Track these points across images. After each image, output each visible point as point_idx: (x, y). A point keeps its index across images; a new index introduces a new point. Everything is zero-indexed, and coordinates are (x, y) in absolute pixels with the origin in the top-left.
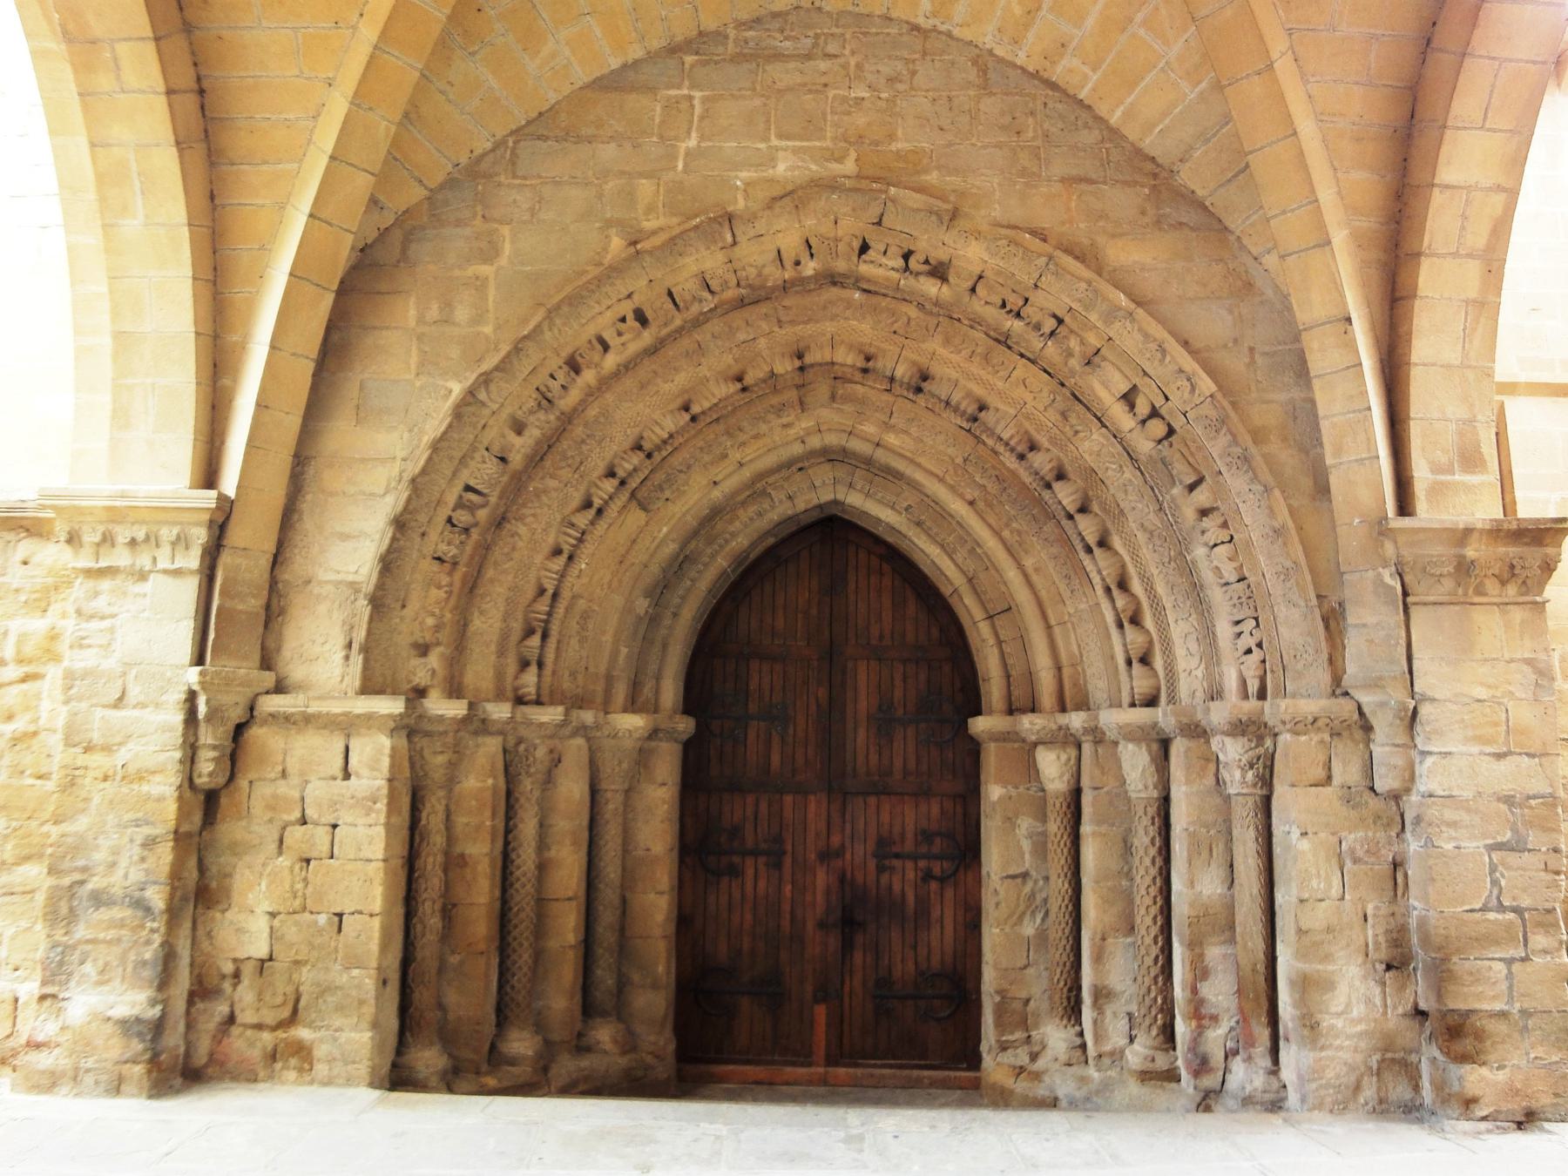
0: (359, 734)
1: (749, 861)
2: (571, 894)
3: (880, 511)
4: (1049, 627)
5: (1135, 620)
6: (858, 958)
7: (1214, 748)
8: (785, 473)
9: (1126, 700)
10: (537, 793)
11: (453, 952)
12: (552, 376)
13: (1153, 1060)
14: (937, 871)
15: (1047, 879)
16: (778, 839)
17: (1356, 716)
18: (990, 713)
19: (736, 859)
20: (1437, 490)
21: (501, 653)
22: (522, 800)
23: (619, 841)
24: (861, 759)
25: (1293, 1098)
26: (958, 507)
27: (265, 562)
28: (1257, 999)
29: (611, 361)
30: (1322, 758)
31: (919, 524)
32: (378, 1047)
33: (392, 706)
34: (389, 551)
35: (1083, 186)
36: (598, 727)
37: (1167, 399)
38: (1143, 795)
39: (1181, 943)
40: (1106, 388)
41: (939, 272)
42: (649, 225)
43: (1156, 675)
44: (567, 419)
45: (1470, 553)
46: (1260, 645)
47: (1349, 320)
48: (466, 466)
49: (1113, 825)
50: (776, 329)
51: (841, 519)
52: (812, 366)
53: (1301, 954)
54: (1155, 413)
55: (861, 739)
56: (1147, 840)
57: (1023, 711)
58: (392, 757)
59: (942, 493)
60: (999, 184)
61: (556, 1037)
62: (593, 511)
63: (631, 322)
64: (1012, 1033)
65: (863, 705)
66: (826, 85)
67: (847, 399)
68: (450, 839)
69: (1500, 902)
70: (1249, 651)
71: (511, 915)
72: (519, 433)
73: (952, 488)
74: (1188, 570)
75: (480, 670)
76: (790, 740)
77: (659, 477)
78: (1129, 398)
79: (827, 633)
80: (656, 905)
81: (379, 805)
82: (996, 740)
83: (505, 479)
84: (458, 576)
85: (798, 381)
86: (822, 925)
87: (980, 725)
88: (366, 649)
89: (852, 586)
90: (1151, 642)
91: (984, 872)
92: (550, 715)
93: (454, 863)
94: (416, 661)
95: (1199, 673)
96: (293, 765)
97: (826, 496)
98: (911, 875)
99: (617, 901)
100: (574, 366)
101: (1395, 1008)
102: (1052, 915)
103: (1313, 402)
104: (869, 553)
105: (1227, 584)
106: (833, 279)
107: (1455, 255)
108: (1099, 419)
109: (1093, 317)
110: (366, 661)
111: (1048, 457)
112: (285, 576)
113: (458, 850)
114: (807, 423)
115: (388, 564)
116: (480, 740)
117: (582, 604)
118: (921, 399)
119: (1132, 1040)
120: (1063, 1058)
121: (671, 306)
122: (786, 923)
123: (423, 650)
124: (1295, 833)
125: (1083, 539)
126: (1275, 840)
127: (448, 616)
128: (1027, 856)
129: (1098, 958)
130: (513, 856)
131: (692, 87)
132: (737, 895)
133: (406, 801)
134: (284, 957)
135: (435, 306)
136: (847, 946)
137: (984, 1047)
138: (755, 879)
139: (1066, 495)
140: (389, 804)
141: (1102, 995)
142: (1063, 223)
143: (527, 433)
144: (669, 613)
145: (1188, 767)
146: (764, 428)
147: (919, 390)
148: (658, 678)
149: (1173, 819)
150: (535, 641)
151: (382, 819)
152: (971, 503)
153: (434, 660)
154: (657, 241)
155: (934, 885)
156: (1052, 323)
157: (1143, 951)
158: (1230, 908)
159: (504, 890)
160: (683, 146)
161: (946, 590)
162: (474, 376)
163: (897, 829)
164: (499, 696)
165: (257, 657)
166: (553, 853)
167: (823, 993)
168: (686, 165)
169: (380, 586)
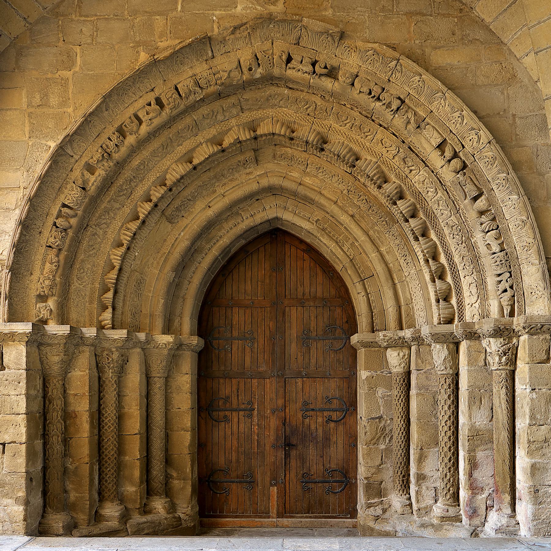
1: (234, 414)
3: (300, 222)
8: (249, 202)
12: (109, 139)
13: (448, 511)
14: (334, 417)
16: (250, 403)
22: (107, 382)
26: (344, 218)
29: (144, 129)
31: (323, 230)
35: (419, 18)
37: (463, 147)
40: (427, 142)
42: (162, 45)
44: (120, 165)
46: (511, 287)
51: (281, 230)
52: (261, 136)
53: (530, 453)
54: (455, 155)
56: (446, 397)
59: (335, 209)
60: (369, 17)
62: (139, 221)
63: (154, 106)
67: (283, 157)
70: (506, 291)
74: (472, 248)
76: (256, 350)
77: (177, 203)
82: (365, 347)
83: (87, 200)
84: (62, 257)
85: (254, 146)
87: (355, 339)
89: (288, 267)
90: (450, 289)
95: (477, 305)
99: (162, 434)
100: (121, 132)
102: (395, 437)
106: (270, 80)
119: (436, 501)
120: (400, 511)
121: (178, 96)
123: (43, 298)
127: (58, 279)
128: (381, 408)
129: (421, 459)
135: (38, 97)
137: (359, 507)
140: (27, 383)
141: (421, 478)
143: (97, 174)
144: (186, 282)
146: (237, 175)
147: (322, 150)
149: (460, 386)
151: (24, 392)
152: (352, 216)
153: (51, 303)
157: (443, 455)
161: (338, 268)
162: (61, 138)
167: (274, 480)
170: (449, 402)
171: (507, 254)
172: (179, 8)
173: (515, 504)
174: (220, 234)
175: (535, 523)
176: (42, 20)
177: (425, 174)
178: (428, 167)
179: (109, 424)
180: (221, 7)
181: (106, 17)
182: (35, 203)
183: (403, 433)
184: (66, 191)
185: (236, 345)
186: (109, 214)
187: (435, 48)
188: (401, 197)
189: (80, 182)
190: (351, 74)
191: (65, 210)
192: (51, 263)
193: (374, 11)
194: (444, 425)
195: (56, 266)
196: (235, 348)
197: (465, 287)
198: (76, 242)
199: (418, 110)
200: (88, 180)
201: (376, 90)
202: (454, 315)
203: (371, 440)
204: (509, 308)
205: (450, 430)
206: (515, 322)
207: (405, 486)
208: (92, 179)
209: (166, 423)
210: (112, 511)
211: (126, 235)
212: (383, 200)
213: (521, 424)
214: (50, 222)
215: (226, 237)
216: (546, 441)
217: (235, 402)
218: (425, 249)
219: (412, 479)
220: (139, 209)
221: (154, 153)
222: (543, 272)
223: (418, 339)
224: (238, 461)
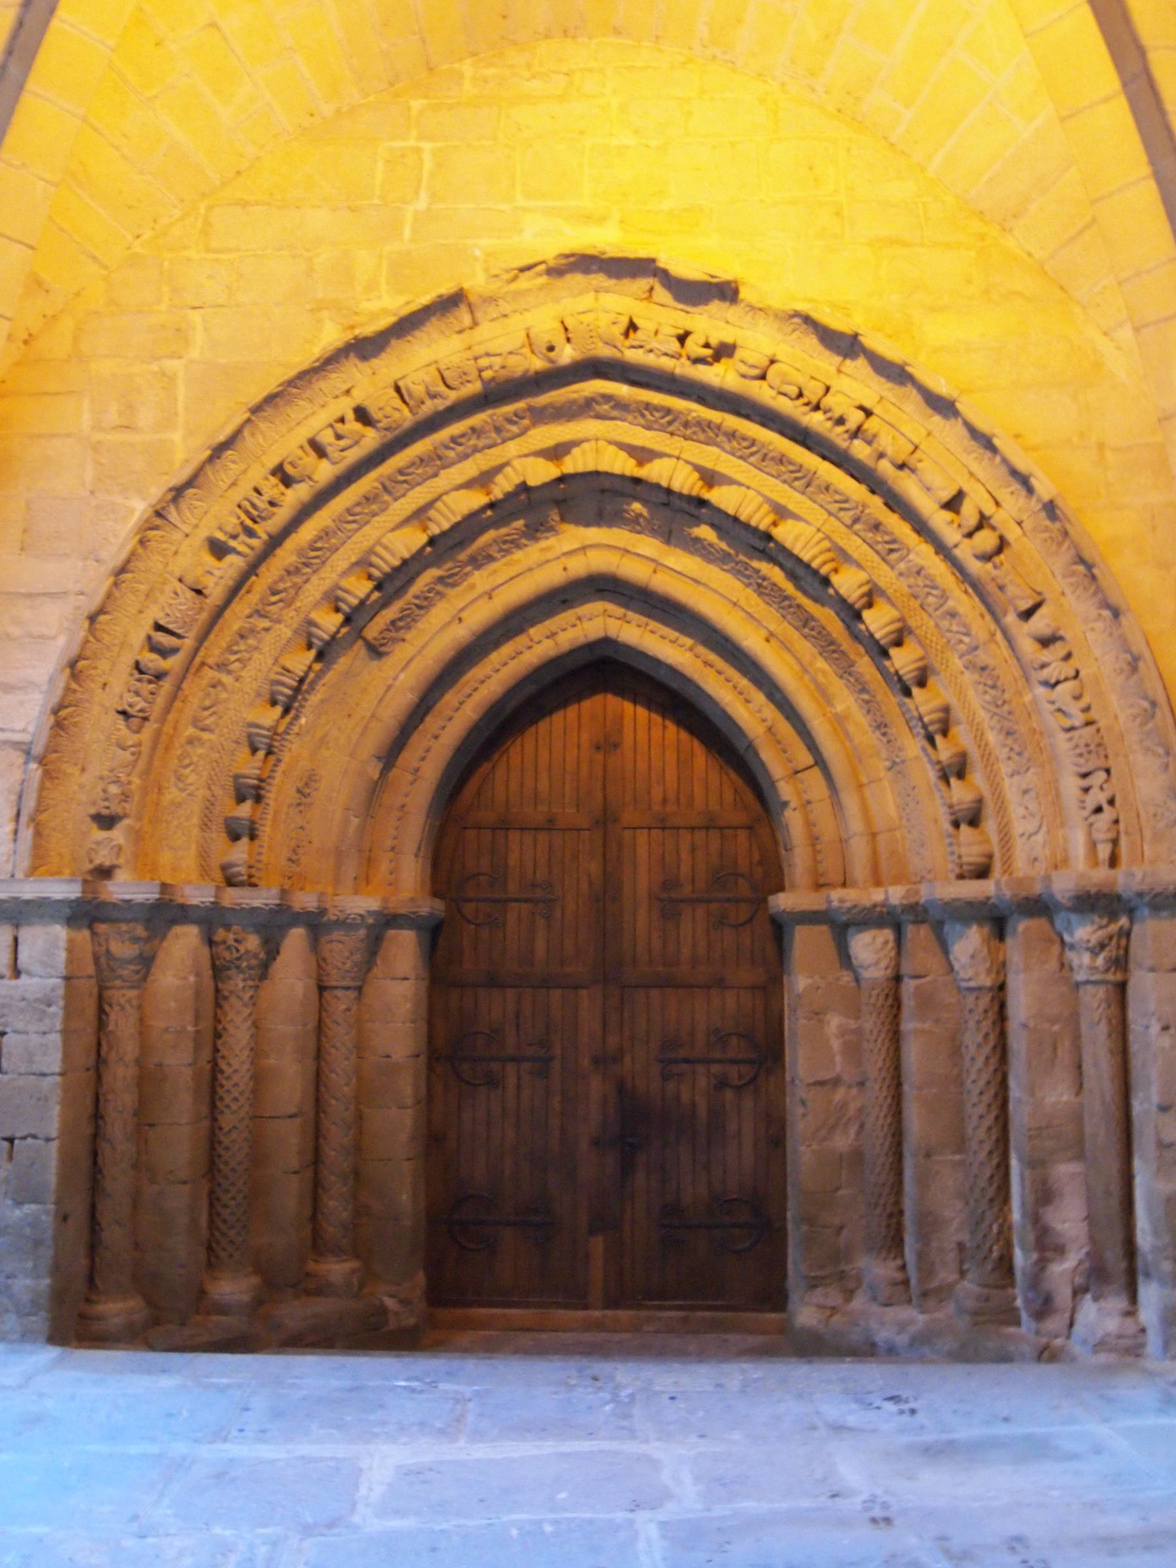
0: (29, 924)
1: (511, 1068)
2: (293, 1110)
6: (640, 1179)
19: (495, 1066)
21: (205, 826)
25: (1153, 1341)
37: (997, 504)
39: (1020, 1160)
46: (1111, 802)
54: (983, 522)
55: (641, 922)
58: (70, 950)
66: (582, 132)
70: (1099, 810)
79: (599, 795)
80: (397, 1124)
81: (53, 1009)
86: (596, 1142)
87: (783, 902)
91: (788, 1078)
93: (149, 1080)
94: (99, 835)
98: (702, 1082)
124: (1155, 1029)
126: (1131, 1037)
128: (838, 1059)
131: (422, 137)
136: (627, 1168)
155: (729, 1094)
158: (1078, 1117)
160: (409, 212)
166: (272, 1061)
170: (987, 1049)
171: (1098, 730)
181: (259, 252)
195: (133, 754)
196: (511, 918)
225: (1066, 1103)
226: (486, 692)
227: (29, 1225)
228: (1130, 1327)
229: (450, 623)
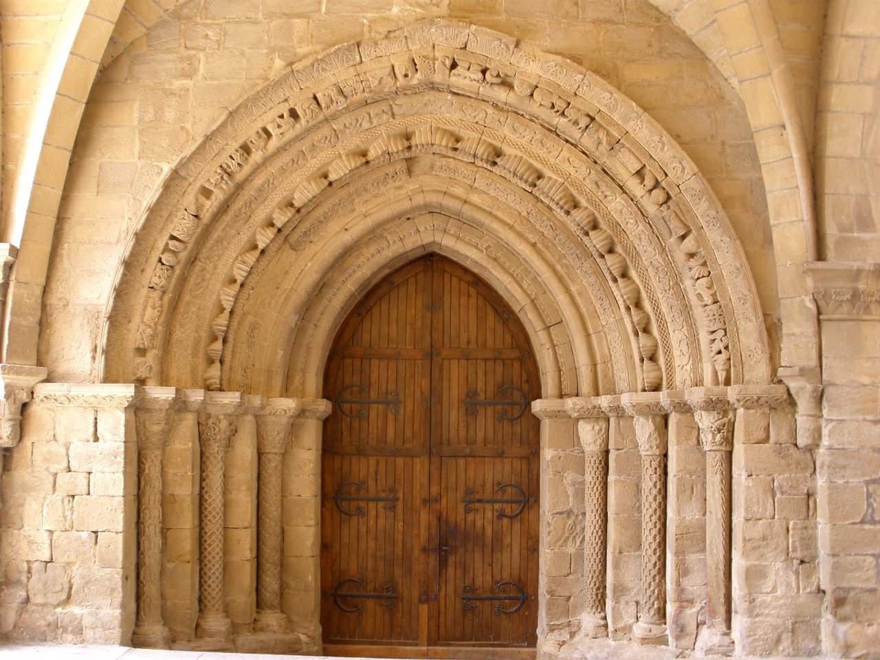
1: (372, 505)
2: (246, 524)
4: (588, 336)
5: (646, 330)
6: (451, 571)
7: (696, 419)
8: (397, 222)
9: (640, 387)
10: (221, 454)
11: (169, 561)
12: (231, 157)
13: (650, 631)
14: (508, 511)
15: (584, 514)
16: (393, 490)
17: (785, 396)
18: (547, 398)
19: (362, 504)
20: (842, 243)
21: (194, 355)
22: (212, 458)
23: (278, 489)
24: (453, 432)
26: (522, 248)
27: (38, 291)
28: (718, 586)
29: (274, 144)
30: (764, 424)
31: (495, 260)
32: (123, 623)
33: (126, 391)
34: (121, 283)
36: (263, 408)
37: (666, 175)
38: (650, 453)
41: (506, 84)
42: (301, 51)
43: (660, 369)
45: (861, 286)
46: (726, 348)
47: (784, 127)
48: (172, 222)
49: (629, 475)
50: (391, 120)
51: (439, 255)
53: (745, 554)
54: (657, 184)
55: (453, 417)
56: (651, 484)
57: (569, 396)
60: (549, 23)
61: (239, 621)
62: (258, 252)
64: (558, 619)
65: (455, 392)
68: (164, 484)
69: (873, 518)
70: (720, 352)
71: (206, 537)
72: (208, 197)
73: (520, 235)
74: (682, 296)
75: (181, 364)
78: (640, 174)
79: (428, 339)
80: (305, 535)
82: (550, 417)
83: (199, 230)
84: (167, 298)
85: (407, 155)
86: (424, 550)
87: (537, 406)
88: (106, 352)
89: (447, 305)
90: (656, 346)
91: (541, 511)
92: (230, 399)
93: (166, 501)
94: (139, 360)
95: (688, 367)
96: (60, 431)
97: (427, 239)
98: (489, 515)
99: (278, 529)
101: (805, 588)
102: (587, 538)
103: (761, 179)
104: (460, 280)
105: (706, 305)
107: (857, 83)
108: (621, 187)
109: (615, 117)
110: (106, 359)
111: (585, 213)
112: (53, 300)
113: (170, 491)
114: (412, 186)
115: (121, 293)
116: (182, 415)
117: (250, 318)
118: (495, 169)
120: (591, 634)
121: (316, 106)
122: (399, 549)
125: (611, 273)
127: (160, 328)
128: (571, 499)
129: (616, 566)
130: (206, 497)
132: (363, 530)
133: (135, 456)
134: (60, 559)
135: (152, 111)
136: (443, 563)
137: (539, 631)
138: (376, 518)
139: (596, 241)
140: (125, 458)
142: (594, 51)
143: (213, 197)
144: (311, 325)
145: (679, 433)
146: (383, 189)
148: (304, 371)
150: (218, 345)
152: (534, 245)
154: (306, 62)
156: (587, 120)
158: (703, 528)
159: (201, 521)
161: (516, 308)
163: (479, 483)
164: (195, 385)
165: (35, 357)
167: (426, 597)
168: (327, 8)
169: (115, 308)
172: (323, 10)
173: (730, 619)
174: (359, 262)
175: (750, 639)
176: (163, 24)
177: (623, 202)
178: (626, 193)
179: (214, 513)
180: (373, 8)
182: (141, 238)
183: (597, 532)
184: (176, 220)
185: (375, 411)
186: (222, 243)
187: (630, 61)
188: (595, 227)
189: (193, 210)
190: (530, 85)
191: (172, 244)
192: (154, 308)
193: (555, 17)
194: (648, 520)
196: (373, 415)
197: (675, 344)
198: (183, 280)
199: (610, 129)
200: (202, 206)
201: (560, 105)
202: (661, 379)
203: (556, 542)
204: (724, 374)
205: (655, 527)
206: (729, 393)
207: (599, 601)
208: (208, 203)
209: (282, 515)
210: (216, 623)
211: (242, 269)
212: (573, 227)
213: (738, 518)
214: (154, 259)
215: (365, 267)
216: (764, 538)
217: (372, 489)
218: (625, 294)
219: (609, 592)
220: (258, 237)
221: (283, 170)
222: (761, 331)
223: (619, 411)
224: (375, 570)
225: (697, 519)
226: (360, 274)
227: (108, 579)
228: (727, 640)
229: (339, 232)
